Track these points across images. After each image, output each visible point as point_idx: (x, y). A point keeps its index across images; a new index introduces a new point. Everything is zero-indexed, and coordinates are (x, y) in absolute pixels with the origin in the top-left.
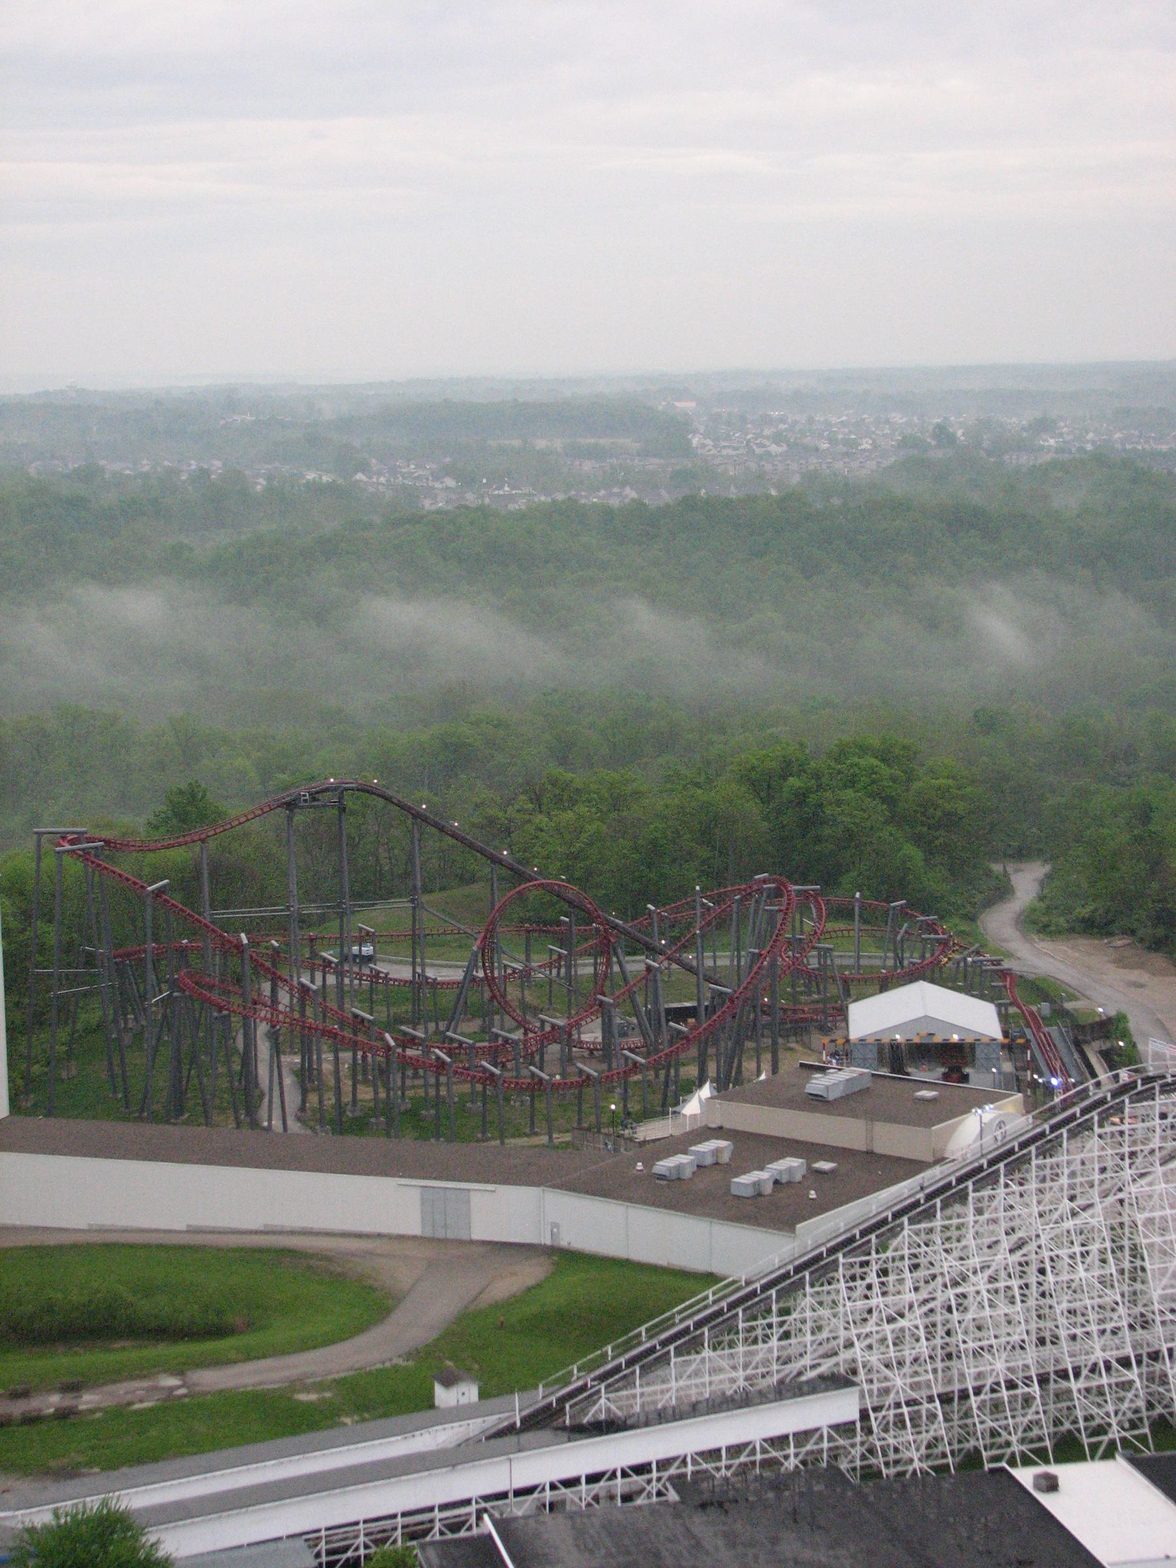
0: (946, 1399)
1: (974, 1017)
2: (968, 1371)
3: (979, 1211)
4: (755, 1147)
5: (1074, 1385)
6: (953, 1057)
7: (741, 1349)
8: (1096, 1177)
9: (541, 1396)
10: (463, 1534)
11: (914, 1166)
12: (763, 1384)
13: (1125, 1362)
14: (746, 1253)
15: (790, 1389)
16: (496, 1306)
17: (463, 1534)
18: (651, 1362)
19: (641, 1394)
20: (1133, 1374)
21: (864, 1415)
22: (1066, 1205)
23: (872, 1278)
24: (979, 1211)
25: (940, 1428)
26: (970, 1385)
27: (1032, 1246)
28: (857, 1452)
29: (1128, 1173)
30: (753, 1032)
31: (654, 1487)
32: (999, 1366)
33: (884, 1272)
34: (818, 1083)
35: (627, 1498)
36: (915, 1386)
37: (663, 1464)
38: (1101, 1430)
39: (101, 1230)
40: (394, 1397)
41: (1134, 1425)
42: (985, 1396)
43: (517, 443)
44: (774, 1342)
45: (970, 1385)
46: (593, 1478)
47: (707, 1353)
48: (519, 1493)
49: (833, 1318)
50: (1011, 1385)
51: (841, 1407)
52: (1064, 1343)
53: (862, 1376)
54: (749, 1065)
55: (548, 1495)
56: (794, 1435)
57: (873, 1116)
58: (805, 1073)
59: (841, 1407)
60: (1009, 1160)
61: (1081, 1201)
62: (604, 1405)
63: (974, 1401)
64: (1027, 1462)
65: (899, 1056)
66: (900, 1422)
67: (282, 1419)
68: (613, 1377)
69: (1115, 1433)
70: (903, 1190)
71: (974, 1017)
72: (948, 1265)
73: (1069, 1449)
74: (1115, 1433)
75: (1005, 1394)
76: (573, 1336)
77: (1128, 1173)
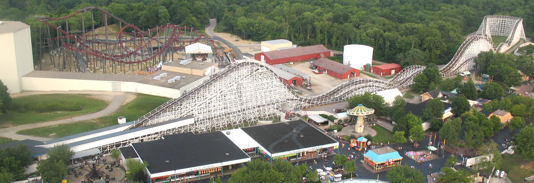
0: (209, 119)
1: (206, 49)
2: (213, 114)
3: (214, 87)
4: (172, 74)
5: (231, 116)
6: (204, 56)
7: (173, 112)
8: (234, 80)
9: (139, 121)
10: (126, 146)
11: (200, 77)
12: (177, 118)
13: (239, 111)
14: (174, 94)
15: (181, 119)
16: (127, 104)
17: (126, 146)
18: (158, 114)
19: (156, 121)
20: (240, 113)
21: (195, 122)
22: (229, 85)
23: (196, 99)
24: (214, 87)
25: (208, 124)
26: (213, 116)
27: (223, 92)
28: (194, 128)
29: (239, 79)
30: (168, 51)
31: (159, 136)
32: (218, 113)
33: (198, 98)
34: (182, 62)
35: (154, 138)
36: (204, 117)
37: (161, 132)
38: (235, 123)
39: (53, 91)
40: (111, 122)
41: (240, 122)
42: (216, 118)
43: (411, 154)
44: (179, 110)
45: (213, 116)
46: (148, 135)
47: (168, 113)
48: (135, 138)
49: (188, 107)
50: (220, 116)
51: (191, 121)
52: (229, 108)
53: (194, 116)
54: (168, 58)
55: (141, 139)
56: (342, 55)
57: (192, 68)
58: (179, 60)
59: (191, 121)
60: (215, 78)
61: (231, 84)
62: (150, 122)
63: (214, 119)
64: (223, 130)
65: (194, 56)
66: (201, 123)
67: (90, 127)
68: (151, 118)
69: (238, 123)
70: (200, 82)
71: (206, 49)
72: (209, 96)
73: (230, 127)
74: (238, 123)
75: (219, 118)
76: (144, 108)
77: (239, 79)
